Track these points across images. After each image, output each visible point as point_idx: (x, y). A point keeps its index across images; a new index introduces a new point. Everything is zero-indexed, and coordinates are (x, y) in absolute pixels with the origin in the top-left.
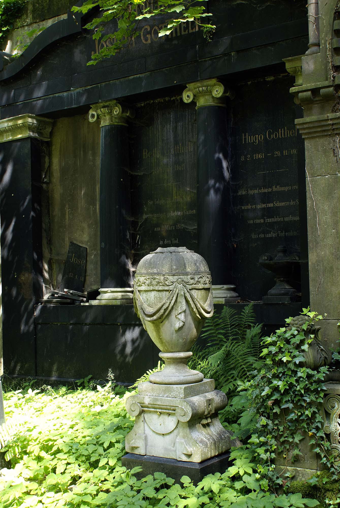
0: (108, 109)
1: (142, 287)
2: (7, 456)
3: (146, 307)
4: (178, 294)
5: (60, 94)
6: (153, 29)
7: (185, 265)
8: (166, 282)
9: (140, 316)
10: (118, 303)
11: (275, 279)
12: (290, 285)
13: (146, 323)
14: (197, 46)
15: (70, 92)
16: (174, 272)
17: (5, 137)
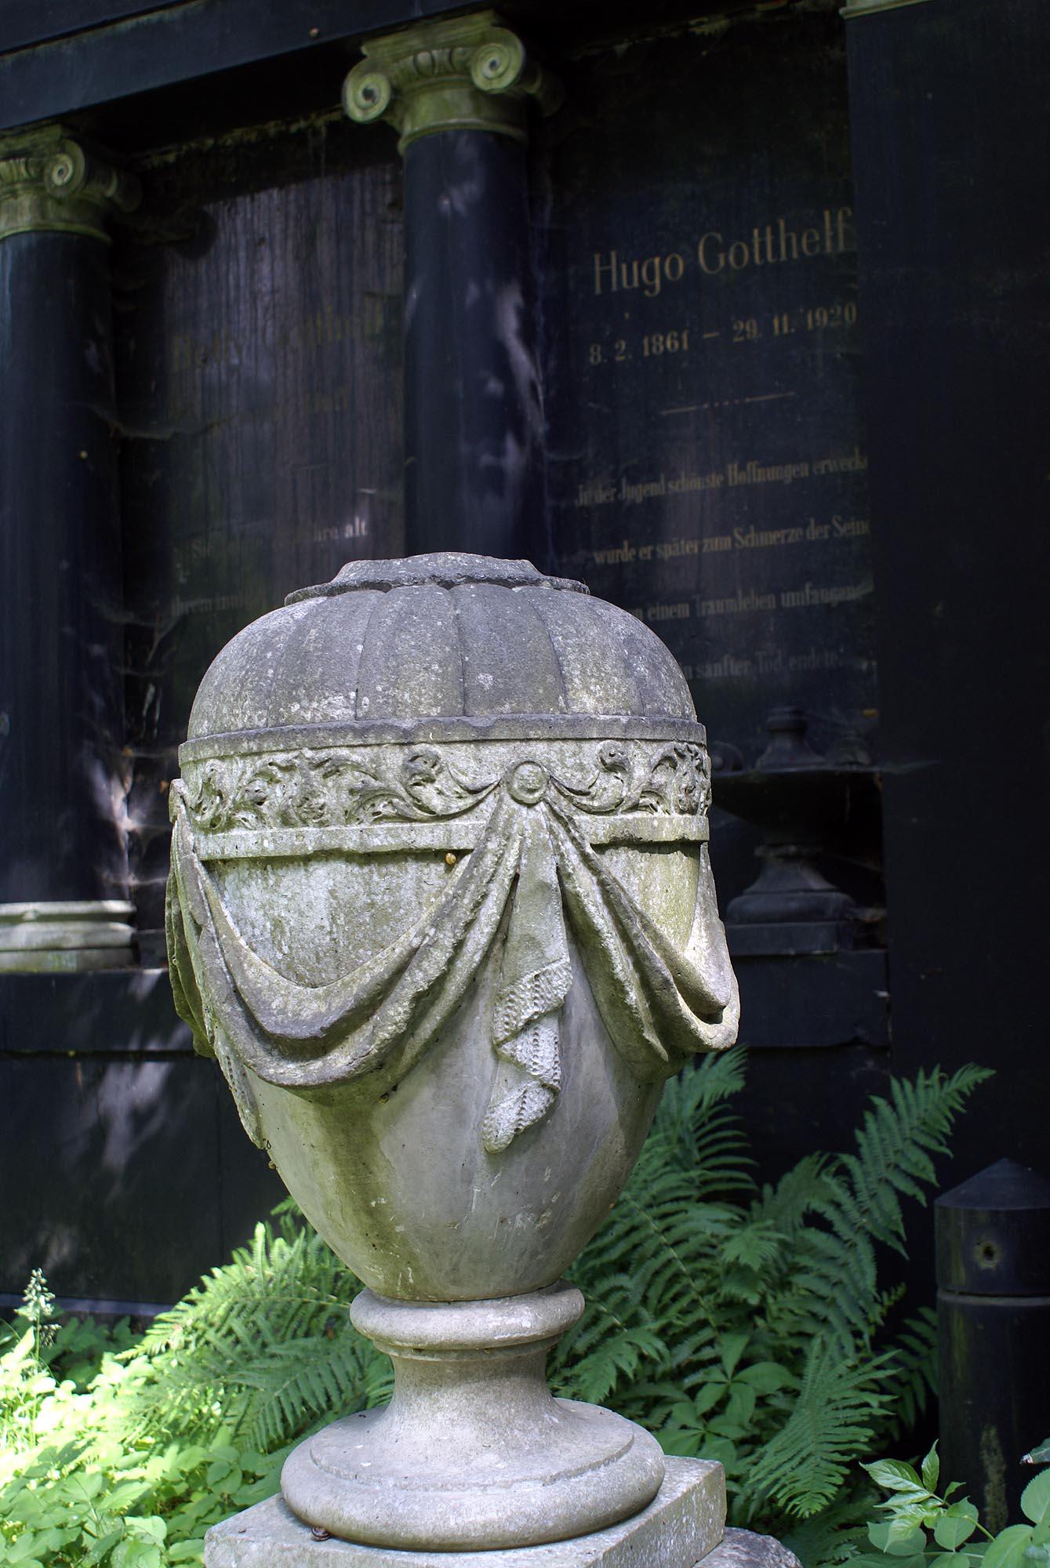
0: (26, 165)
1: (235, 832)
3: (262, 984)
4: (515, 879)
7: (560, 665)
8: (428, 794)
9: (221, 1050)
10: (68, 963)
11: (759, 852)
12: (826, 874)
13: (260, 1101)
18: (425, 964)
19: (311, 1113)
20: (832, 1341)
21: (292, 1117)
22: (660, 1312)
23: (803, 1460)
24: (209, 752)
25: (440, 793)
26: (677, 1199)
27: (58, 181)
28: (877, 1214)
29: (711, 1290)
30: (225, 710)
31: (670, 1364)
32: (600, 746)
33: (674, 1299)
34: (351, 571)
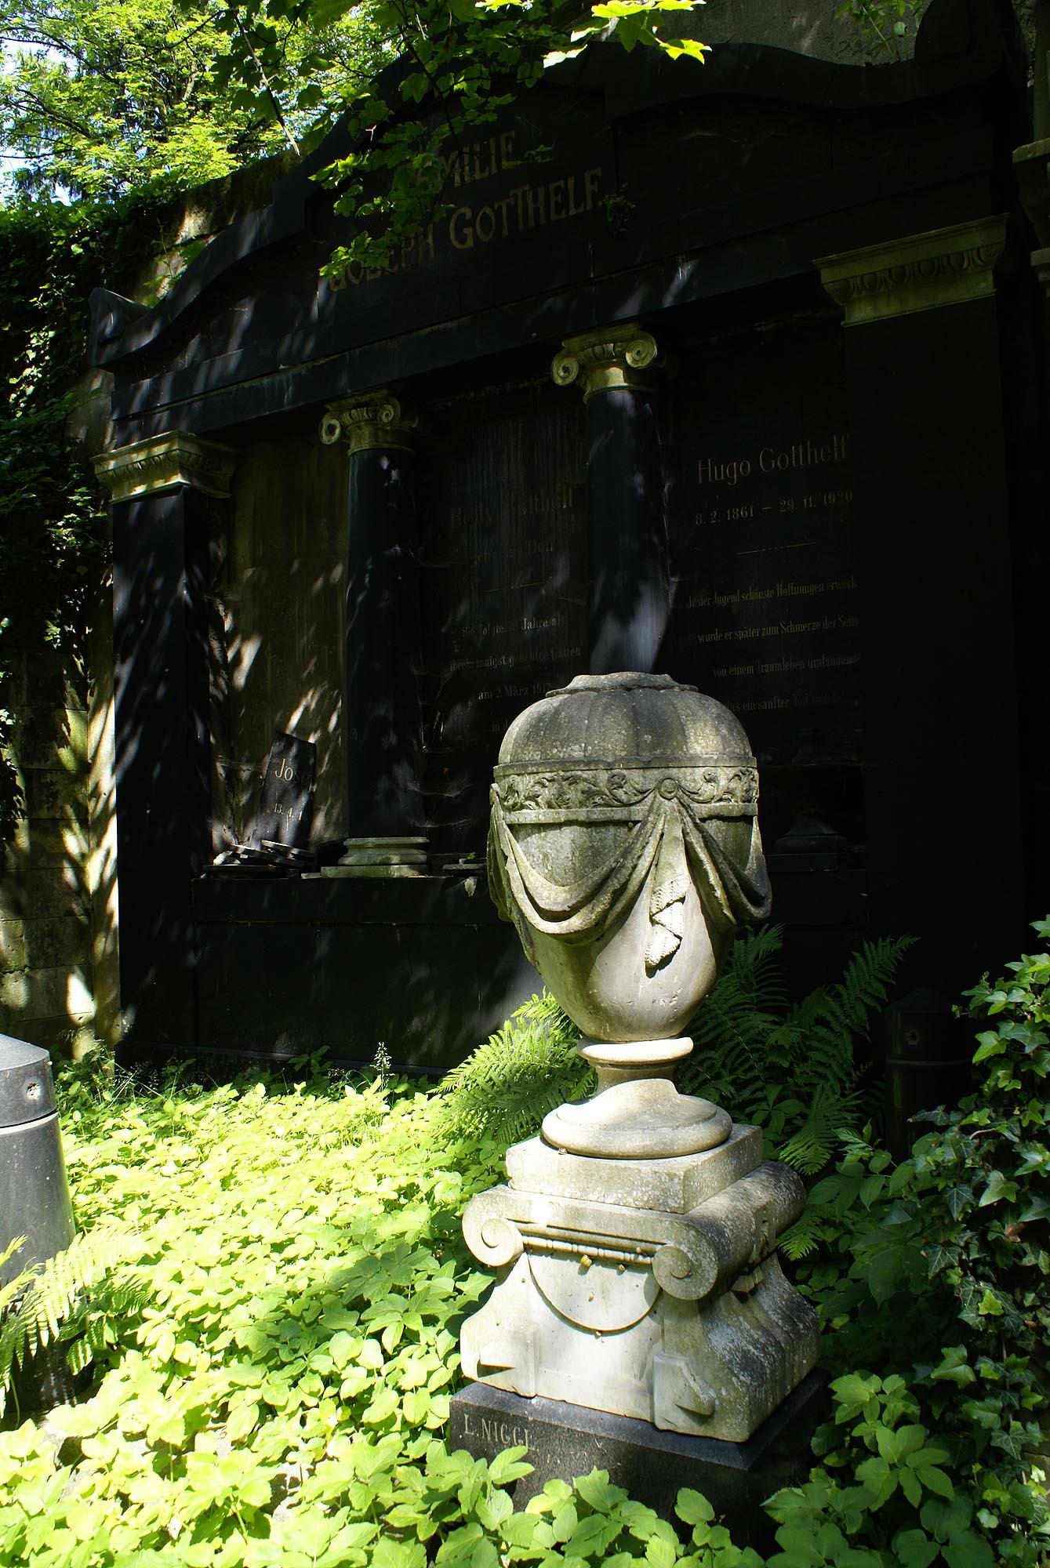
1: (524, 811)
2: (70, 1357)
5: (255, 383)
6: (480, 214)
13: (535, 941)
14: (590, 247)
15: (277, 378)
16: (646, 756)
17: (126, 489)
18: (618, 876)
19: (561, 947)
20: (828, 1088)
21: (551, 950)
22: (733, 1070)
23: (809, 1147)
24: (512, 772)
25: (626, 793)
26: (744, 1010)
27: (385, 420)
28: (854, 1017)
29: (761, 1060)
30: (519, 751)
31: (738, 1100)
32: (703, 770)
33: (741, 1065)
34: (580, 680)
